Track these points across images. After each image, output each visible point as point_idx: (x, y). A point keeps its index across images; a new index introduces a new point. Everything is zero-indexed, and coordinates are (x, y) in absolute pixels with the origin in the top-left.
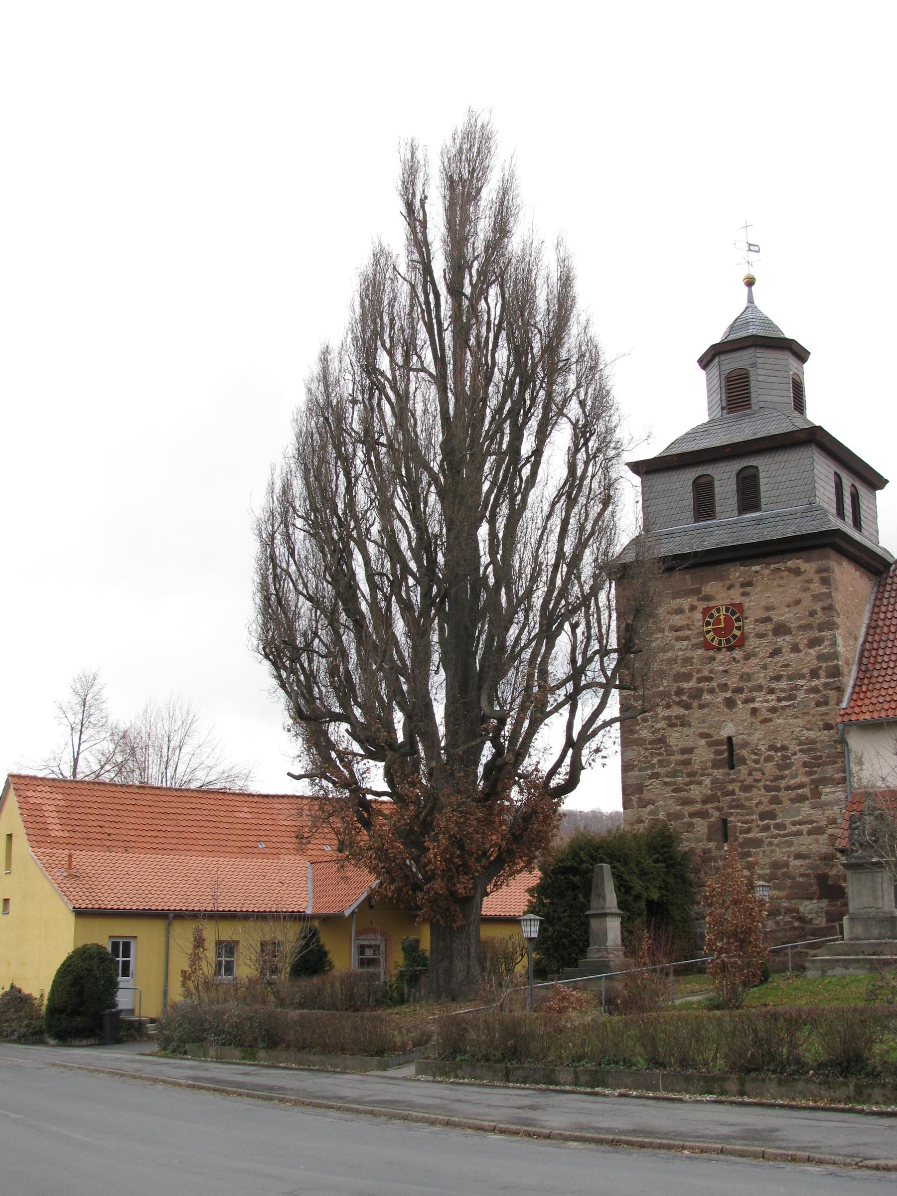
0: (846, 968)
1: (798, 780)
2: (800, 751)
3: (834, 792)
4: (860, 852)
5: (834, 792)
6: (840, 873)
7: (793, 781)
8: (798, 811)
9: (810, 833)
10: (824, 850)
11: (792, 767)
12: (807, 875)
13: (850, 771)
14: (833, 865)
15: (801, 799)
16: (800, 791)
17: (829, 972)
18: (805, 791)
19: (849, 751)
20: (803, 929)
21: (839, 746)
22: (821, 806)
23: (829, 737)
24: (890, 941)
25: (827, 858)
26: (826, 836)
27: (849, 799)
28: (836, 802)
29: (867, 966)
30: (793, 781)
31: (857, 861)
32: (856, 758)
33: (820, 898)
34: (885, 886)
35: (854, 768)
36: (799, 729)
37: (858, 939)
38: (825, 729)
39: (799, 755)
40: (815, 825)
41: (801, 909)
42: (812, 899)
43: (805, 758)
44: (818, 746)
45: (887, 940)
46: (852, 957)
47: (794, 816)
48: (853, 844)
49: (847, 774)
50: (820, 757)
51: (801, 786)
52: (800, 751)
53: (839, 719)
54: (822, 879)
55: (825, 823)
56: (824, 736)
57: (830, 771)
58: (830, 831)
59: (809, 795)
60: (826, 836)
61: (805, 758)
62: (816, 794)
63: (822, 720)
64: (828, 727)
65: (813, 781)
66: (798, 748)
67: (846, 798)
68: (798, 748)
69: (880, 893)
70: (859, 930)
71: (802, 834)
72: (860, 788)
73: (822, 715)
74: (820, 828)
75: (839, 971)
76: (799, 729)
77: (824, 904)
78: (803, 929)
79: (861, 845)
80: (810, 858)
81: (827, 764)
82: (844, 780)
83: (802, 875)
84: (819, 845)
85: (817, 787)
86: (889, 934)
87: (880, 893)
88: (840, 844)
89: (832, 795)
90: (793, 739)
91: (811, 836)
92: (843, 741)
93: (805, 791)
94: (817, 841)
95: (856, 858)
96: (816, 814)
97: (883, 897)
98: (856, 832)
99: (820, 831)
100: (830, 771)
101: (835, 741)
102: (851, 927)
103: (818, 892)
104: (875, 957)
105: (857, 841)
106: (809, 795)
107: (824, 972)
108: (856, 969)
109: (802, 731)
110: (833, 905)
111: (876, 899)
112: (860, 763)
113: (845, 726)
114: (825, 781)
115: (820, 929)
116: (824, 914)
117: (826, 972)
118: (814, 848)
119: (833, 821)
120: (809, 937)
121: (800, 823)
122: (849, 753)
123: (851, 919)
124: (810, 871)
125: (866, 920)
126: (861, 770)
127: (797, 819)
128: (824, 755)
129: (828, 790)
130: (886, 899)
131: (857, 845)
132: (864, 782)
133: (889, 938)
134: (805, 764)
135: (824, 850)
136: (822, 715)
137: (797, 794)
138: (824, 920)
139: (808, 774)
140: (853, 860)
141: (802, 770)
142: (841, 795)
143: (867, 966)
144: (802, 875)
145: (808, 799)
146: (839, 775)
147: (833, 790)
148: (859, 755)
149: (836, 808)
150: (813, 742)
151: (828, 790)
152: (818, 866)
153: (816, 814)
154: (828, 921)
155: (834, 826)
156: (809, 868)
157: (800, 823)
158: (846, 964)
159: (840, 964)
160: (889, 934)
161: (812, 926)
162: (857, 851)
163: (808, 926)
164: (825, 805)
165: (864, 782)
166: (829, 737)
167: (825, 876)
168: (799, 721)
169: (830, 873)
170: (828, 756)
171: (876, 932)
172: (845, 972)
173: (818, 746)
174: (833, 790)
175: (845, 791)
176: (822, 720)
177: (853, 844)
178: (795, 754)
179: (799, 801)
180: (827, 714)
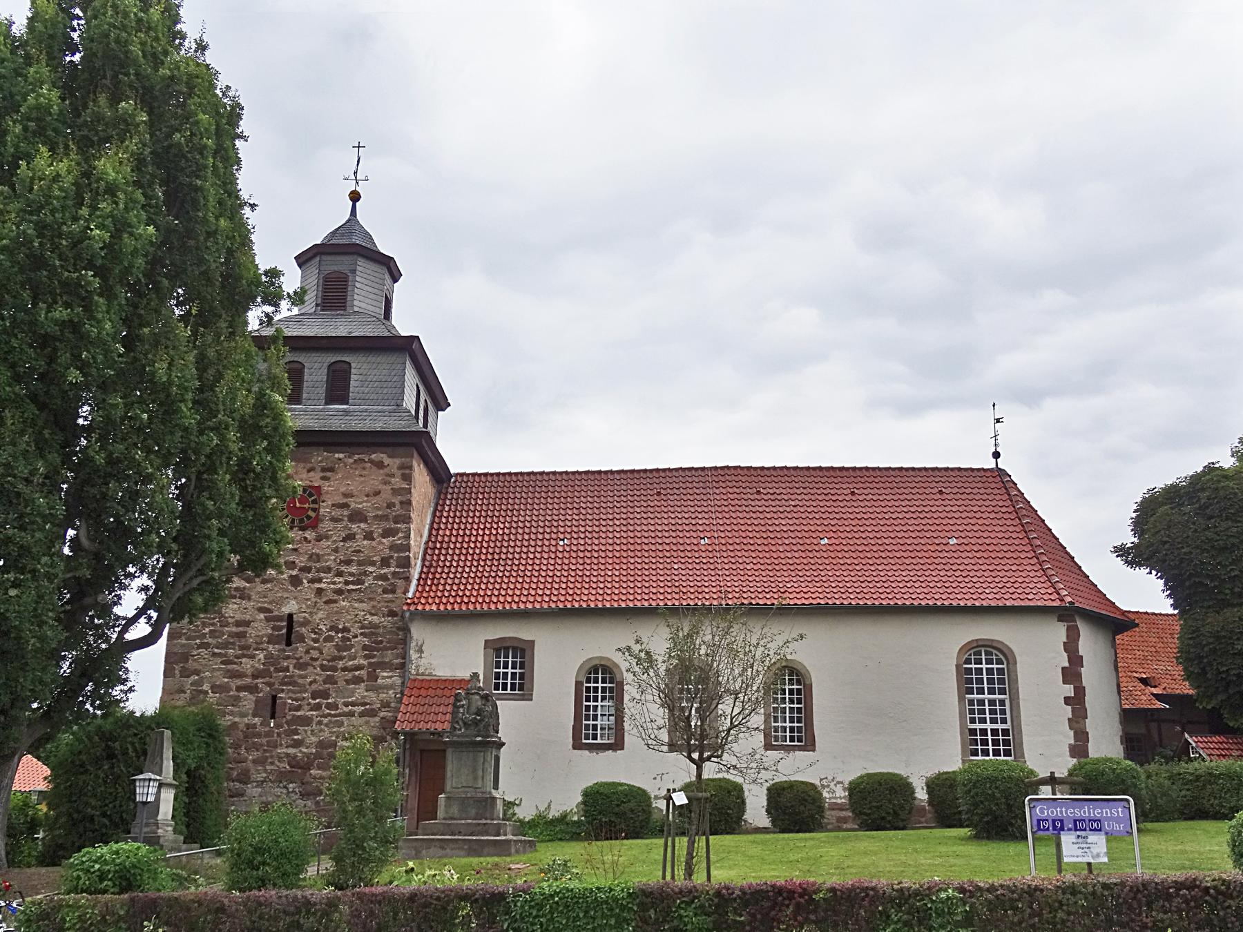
5: (390, 677)
8: (353, 693)
9: (362, 715)
15: (357, 681)
19: (411, 638)
22: (377, 689)
28: (391, 687)
31: (461, 739)
35: (414, 655)
50: (381, 642)
53: (405, 608)
56: (387, 621)
57: (389, 656)
58: (382, 714)
60: (377, 719)
61: (366, 641)
62: (373, 677)
65: (370, 664)
69: (480, 773)
79: (465, 723)
81: (387, 649)
82: (403, 666)
87: (480, 773)
92: (406, 630)
96: (372, 696)
99: (372, 713)
100: (389, 656)
101: (398, 629)
111: (475, 779)
112: (420, 651)
114: (383, 665)
121: (353, 704)
134: (365, 648)
137: (354, 676)
150: (376, 626)
157: (353, 704)
178: (356, 636)
179: (354, 683)
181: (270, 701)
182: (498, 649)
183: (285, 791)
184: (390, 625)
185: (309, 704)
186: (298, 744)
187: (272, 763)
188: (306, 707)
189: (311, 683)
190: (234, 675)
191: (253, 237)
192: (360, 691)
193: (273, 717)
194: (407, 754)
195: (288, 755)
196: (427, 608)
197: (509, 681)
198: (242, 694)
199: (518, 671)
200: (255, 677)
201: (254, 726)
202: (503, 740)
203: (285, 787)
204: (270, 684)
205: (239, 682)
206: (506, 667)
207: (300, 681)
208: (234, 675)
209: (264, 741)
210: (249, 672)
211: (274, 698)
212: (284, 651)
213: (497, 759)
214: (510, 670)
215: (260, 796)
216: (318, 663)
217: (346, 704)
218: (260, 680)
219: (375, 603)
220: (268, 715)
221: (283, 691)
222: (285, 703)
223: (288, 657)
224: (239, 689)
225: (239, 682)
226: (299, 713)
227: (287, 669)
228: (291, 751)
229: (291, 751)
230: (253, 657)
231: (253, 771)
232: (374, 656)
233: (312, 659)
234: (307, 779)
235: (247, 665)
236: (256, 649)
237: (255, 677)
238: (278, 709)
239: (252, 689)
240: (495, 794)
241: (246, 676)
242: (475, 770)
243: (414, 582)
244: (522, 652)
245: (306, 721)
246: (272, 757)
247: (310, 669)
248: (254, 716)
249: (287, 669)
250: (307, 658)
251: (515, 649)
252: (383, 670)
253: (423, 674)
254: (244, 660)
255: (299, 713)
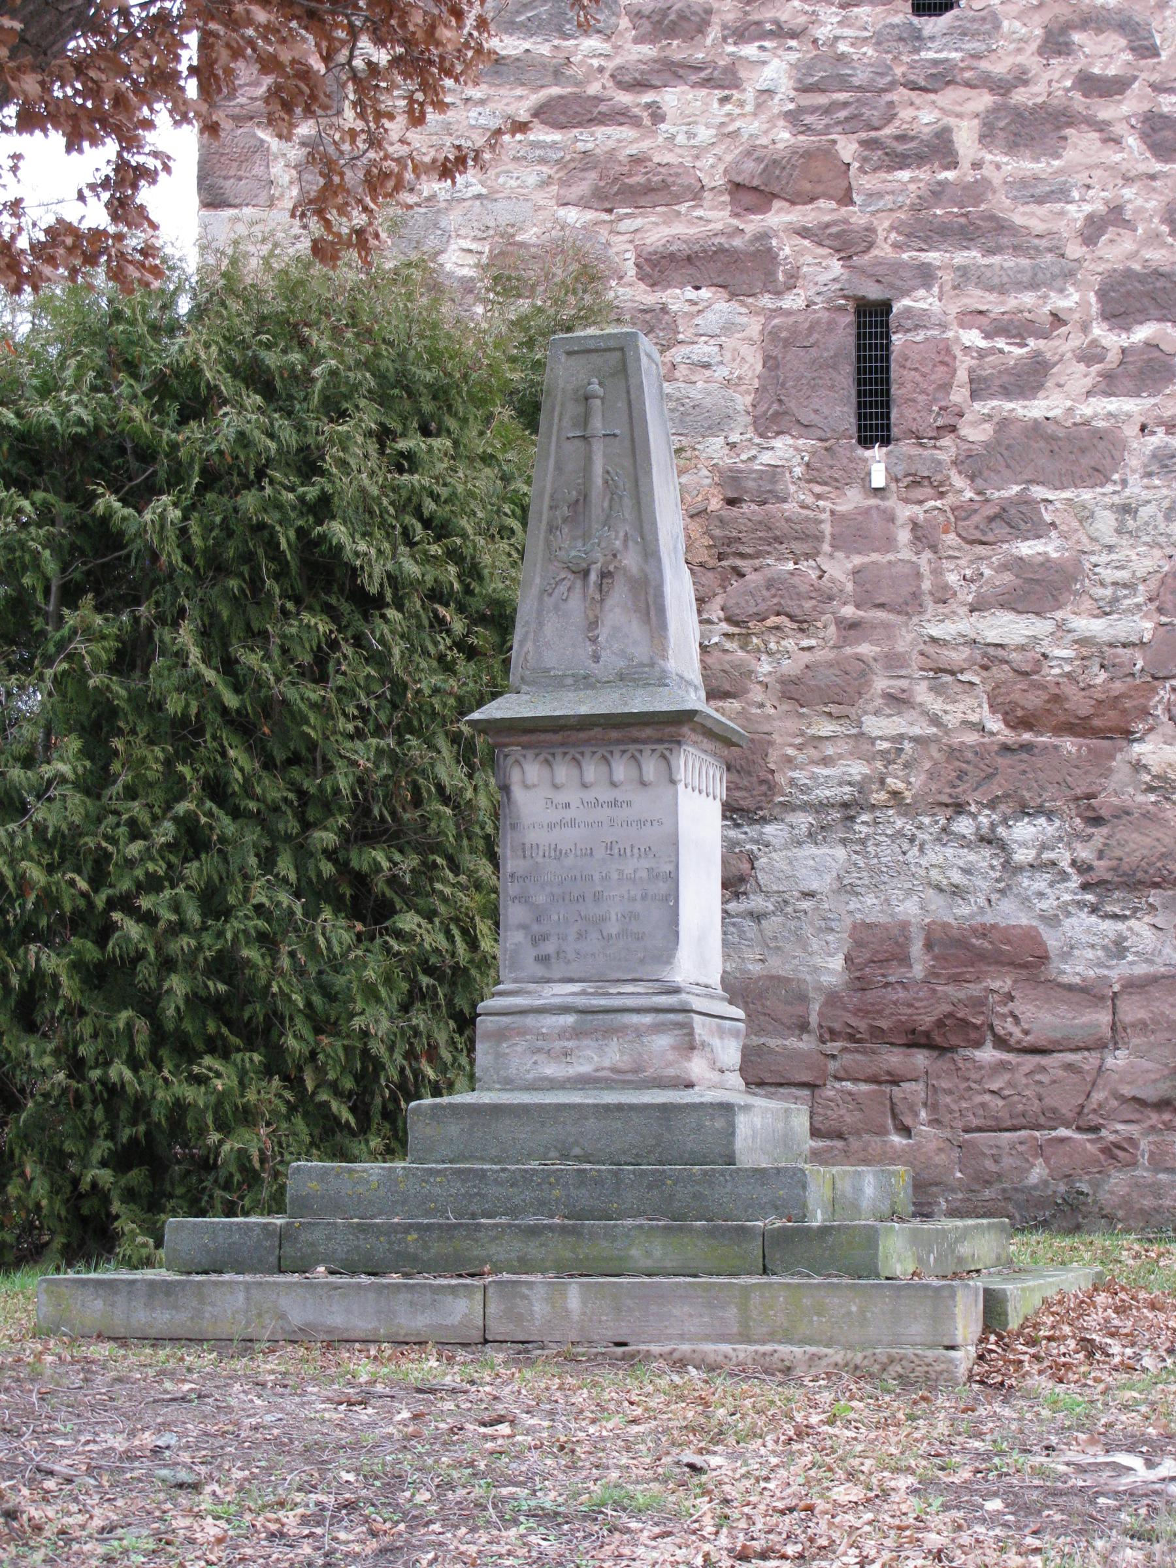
181: (843, 334)
183: (983, 858)
185: (1091, 355)
186: (1040, 589)
187: (899, 701)
188: (1080, 377)
189: (1093, 229)
190: (630, 188)
193: (874, 427)
195: (991, 656)
198: (678, 298)
200: (750, 194)
201: (768, 487)
203: (987, 840)
204: (846, 244)
205: (659, 229)
207: (1029, 217)
208: (630, 188)
209: (838, 568)
210: (712, 172)
211: (873, 321)
212: (917, 39)
215: (846, 889)
216: (1129, 105)
217: (515, 981)
218: (779, 217)
220: (842, 413)
221: (926, 275)
222: (945, 355)
223: (940, 78)
224: (659, 267)
225: (659, 229)
226: (1035, 409)
227: (940, 149)
228: (1007, 628)
229: (1007, 628)
230: (723, 80)
231: (784, 745)
233: (1091, 85)
234: (1119, 789)
235: (693, 129)
236: (742, 33)
237: (750, 194)
238: (904, 382)
239: (738, 269)
241: (696, 193)
243: (679, 588)
245: (1083, 454)
246: (894, 662)
247: (1081, 146)
248: (770, 422)
249: (940, 149)
250: (1050, 82)
254: (671, 98)
255: (1035, 409)
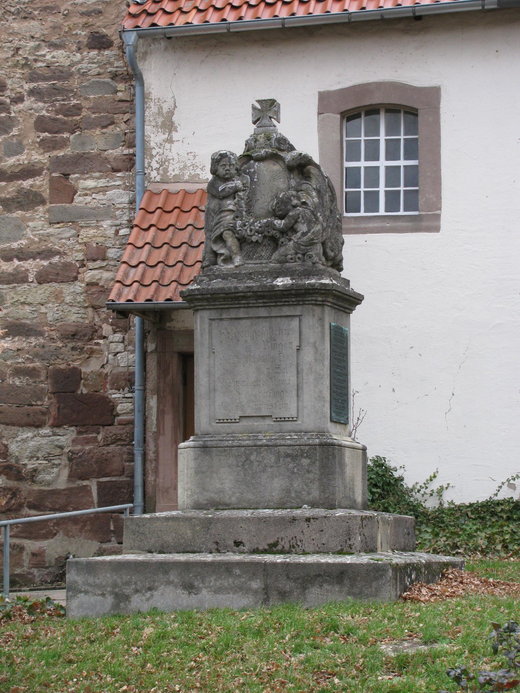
0: (190, 588)
1: (23, 158)
2: (32, 92)
3: (104, 190)
4: (238, 260)
5: (104, 190)
6: (107, 370)
7: (11, 161)
8: (19, 227)
9: (42, 279)
10: (74, 317)
11: (11, 127)
12: (32, 373)
13: (144, 141)
14: (92, 352)
15: (29, 200)
16: (27, 184)
17: (137, 602)
18: (39, 183)
19: (144, 97)
20: (15, 493)
21: (121, 86)
22: (74, 220)
23: (102, 65)
24: (321, 512)
25: (81, 337)
26: (79, 287)
27: (141, 203)
28: (108, 212)
29: (256, 584)
30: (11, 161)
31: (231, 284)
32: (160, 113)
33: (57, 425)
34: (308, 355)
35: (155, 137)
36: (32, 44)
37: (218, 505)
38: (91, 47)
39: (28, 102)
40: (56, 259)
41: (13, 448)
42: (39, 425)
43: (42, 109)
44: (75, 83)
45: (306, 511)
46: (209, 558)
47: (9, 240)
48: (220, 239)
49: (138, 150)
50: (78, 108)
51: (29, 172)
52: (32, 92)
53: (128, 24)
54: (66, 381)
55: (80, 256)
56: (89, 61)
57: (97, 141)
58: (88, 276)
59: (46, 194)
60: (79, 287)
61: (42, 109)
62: (63, 190)
63: (86, 25)
64: (99, 42)
65: (57, 162)
66: (27, 86)
67: (132, 202)
68: (27, 86)
69: (290, 377)
70: (225, 481)
71: (24, 280)
72: (162, 182)
73: (87, 14)
74: (67, 266)
75: (168, 597)
76: (32, 44)
77: (67, 437)
78: (15, 493)
79: (242, 241)
80: (40, 334)
81: (91, 125)
82: (129, 163)
83: (18, 372)
84: (63, 306)
85: (66, 176)
86: (315, 493)
87: (290, 377)
88: (119, 295)
89: (100, 196)
90: (16, 65)
91: (45, 286)
92: (133, 76)
93: (39, 183)
94: (58, 296)
95: (225, 277)
96: (61, 236)
97: (299, 388)
98: (230, 204)
99: (67, 274)
100: (97, 141)
101: (114, 76)
102: (201, 472)
103: (54, 411)
104: (279, 559)
105: (233, 229)
106: (46, 194)
107: (121, 598)
108: (218, 591)
109: (38, 48)
110: (88, 441)
111: (278, 393)
112: (168, 125)
113: (140, 36)
114: (83, 163)
115: (55, 492)
116: (64, 460)
117: (127, 598)
118: (51, 312)
119: (97, 255)
120: (26, 510)
121: (22, 255)
122: (144, 103)
123: (205, 449)
124: (38, 364)
125: (248, 454)
126: (170, 141)
127: (15, 245)
128: (85, 104)
129: (91, 183)
130: (308, 396)
131: (231, 241)
132: (173, 170)
133: (313, 505)
134: (41, 124)
135: (73, 318)
136: (87, 14)
137: (20, 191)
138: (66, 472)
139: (46, 146)
140: (217, 284)
141: (33, 137)
142: (120, 197)
143: (256, 584)
144: (18, 372)
145: (43, 202)
146: (122, 151)
147: (102, 183)
148: (166, 108)
149: (106, 224)
150: (62, 74)
151: (91, 183)
152: (56, 354)
153: (61, 236)
154: (71, 477)
155: (99, 263)
156: (36, 355)
157: (22, 255)
158: (190, 577)
159: (173, 576)
160: (315, 493)
161: (36, 487)
162: (228, 259)
163: (25, 487)
164: (82, 216)
165: (173, 170)
166: (102, 65)
167: (73, 376)
168: (33, 26)
169: (83, 370)
170: (94, 109)
171: (275, 486)
172: (185, 600)
173: (75, 83)
174: (102, 183)
175: (130, 188)
176: (86, 25)
177: (220, 239)
178: (19, 99)
179: (21, 206)
180: (100, 12)
182: (355, 110)
184: (95, 69)
191: (457, 503)
192: (36, 225)
194: (152, 363)
196: (179, 21)
197: (382, 189)
199: (402, 163)
202: (356, 287)
206: (372, 155)
213: (340, 343)
214: (382, 163)
219: (59, 19)
232: (64, 143)
240: (338, 435)
242: (276, 369)
244: (408, 114)
251: (392, 110)
252: (85, 173)
253: (177, 180)
